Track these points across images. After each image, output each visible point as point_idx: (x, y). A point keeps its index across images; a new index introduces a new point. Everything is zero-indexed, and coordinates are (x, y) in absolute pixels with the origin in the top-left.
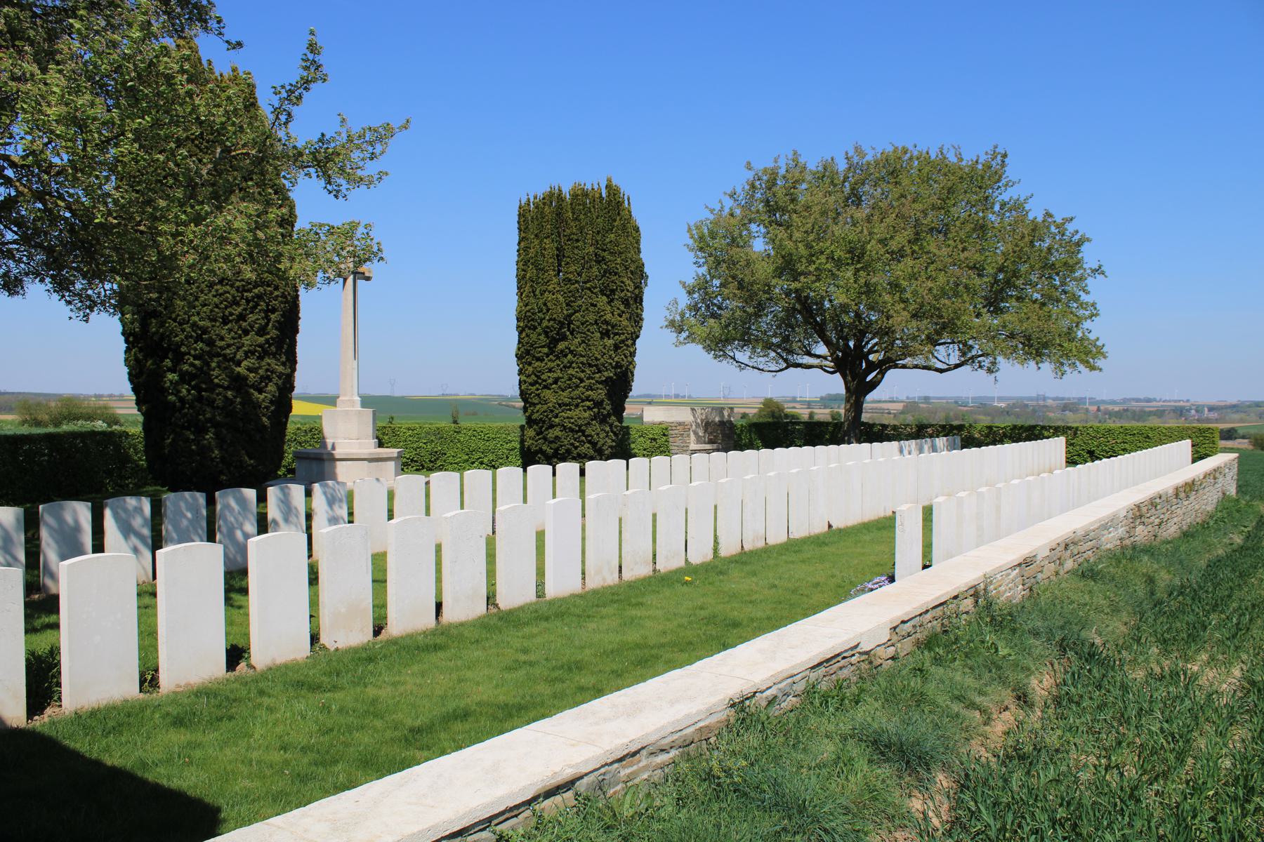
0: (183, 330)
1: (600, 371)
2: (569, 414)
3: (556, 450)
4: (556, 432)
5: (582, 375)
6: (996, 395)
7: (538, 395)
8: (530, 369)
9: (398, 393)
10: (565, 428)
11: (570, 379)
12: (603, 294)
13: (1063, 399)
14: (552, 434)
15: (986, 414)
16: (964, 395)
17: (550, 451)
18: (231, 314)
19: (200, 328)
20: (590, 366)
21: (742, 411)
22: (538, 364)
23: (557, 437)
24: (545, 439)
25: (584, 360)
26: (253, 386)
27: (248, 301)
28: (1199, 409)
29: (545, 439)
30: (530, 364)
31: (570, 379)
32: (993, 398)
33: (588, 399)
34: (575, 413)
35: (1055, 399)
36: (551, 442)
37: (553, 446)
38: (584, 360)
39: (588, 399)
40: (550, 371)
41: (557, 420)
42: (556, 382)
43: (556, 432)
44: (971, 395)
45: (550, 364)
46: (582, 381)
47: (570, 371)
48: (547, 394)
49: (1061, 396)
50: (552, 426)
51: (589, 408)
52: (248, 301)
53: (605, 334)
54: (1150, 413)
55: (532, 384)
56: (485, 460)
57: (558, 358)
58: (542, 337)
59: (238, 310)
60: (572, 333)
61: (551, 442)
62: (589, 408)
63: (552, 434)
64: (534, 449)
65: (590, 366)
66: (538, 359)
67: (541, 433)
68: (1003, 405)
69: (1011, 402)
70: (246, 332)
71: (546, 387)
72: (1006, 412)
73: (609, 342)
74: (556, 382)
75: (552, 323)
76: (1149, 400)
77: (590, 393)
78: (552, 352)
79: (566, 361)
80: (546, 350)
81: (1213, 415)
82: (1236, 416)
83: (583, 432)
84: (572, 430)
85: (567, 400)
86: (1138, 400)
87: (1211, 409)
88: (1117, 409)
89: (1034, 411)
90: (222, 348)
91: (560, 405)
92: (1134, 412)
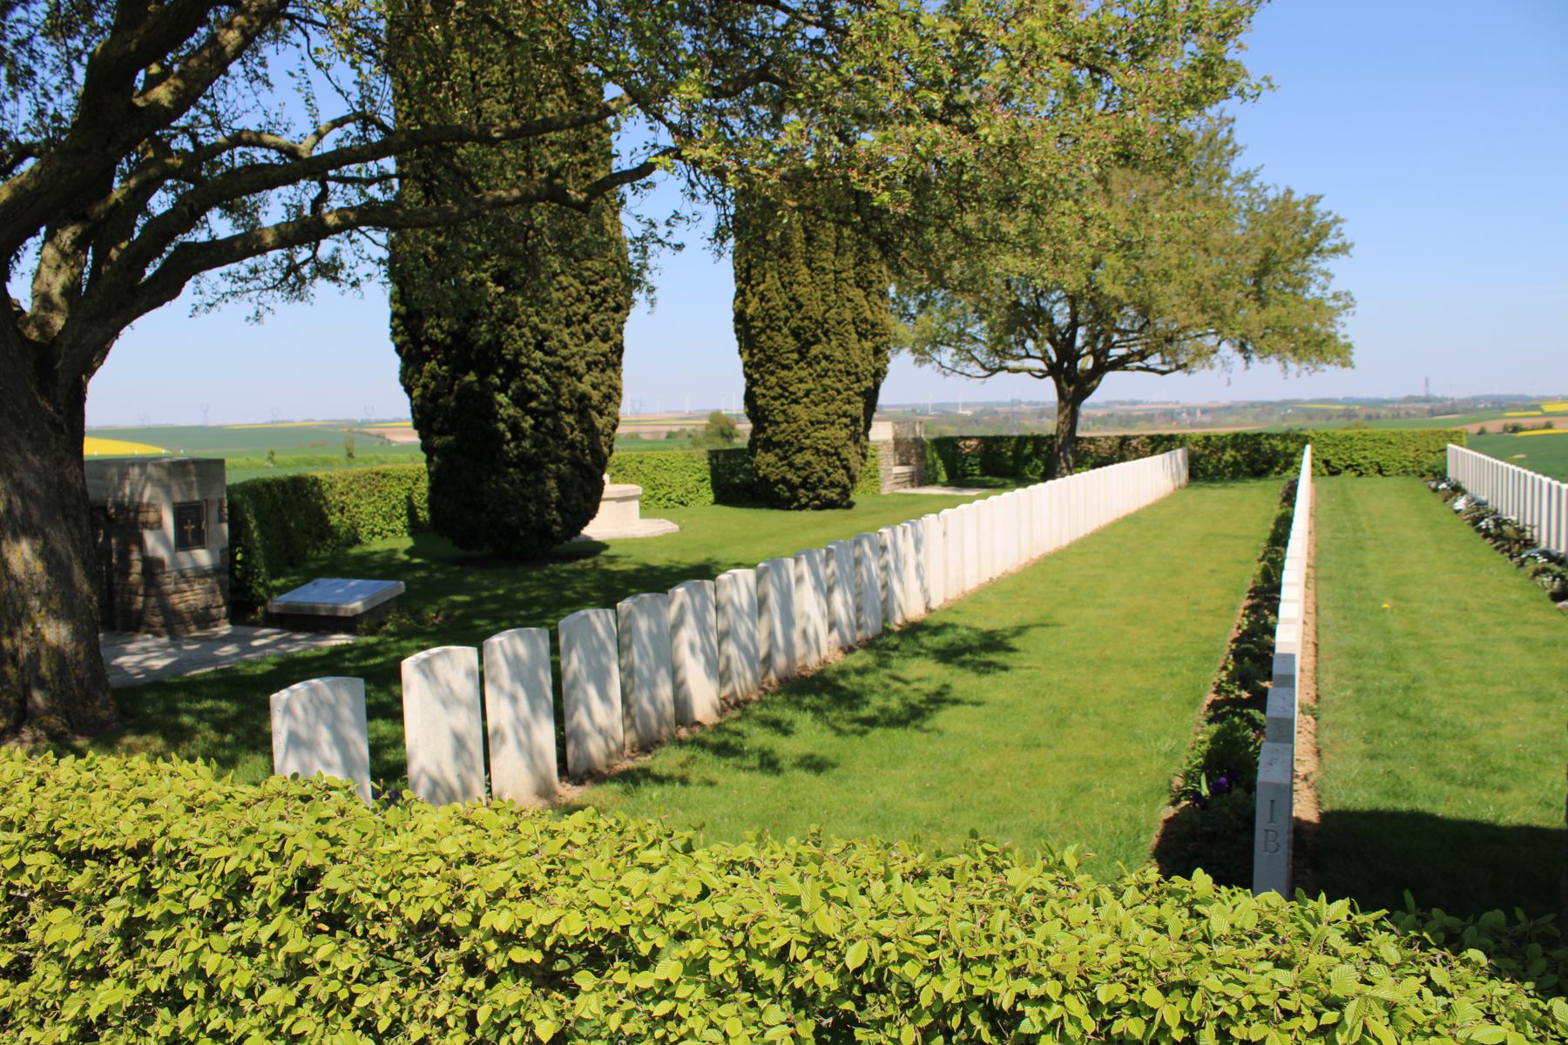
0: (522, 335)
1: (858, 381)
2: (823, 433)
3: (805, 479)
4: (808, 456)
5: (839, 386)
6: (960, 401)
7: (784, 412)
8: (773, 380)
9: (214, 420)
10: (818, 450)
11: (825, 391)
12: (858, 286)
13: (1037, 404)
14: (799, 459)
15: (952, 424)
16: (922, 402)
17: (796, 480)
18: (576, 314)
19: (541, 332)
20: (849, 374)
21: (667, 429)
22: (784, 373)
23: (809, 463)
24: (791, 465)
25: (842, 367)
26: (594, 408)
27: (593, 296)
28: (1191, 412)
29: (791, 465)
30: (772, 373)
31: (825, 391)
32: (956, 405)
33: (845, 415)
34: (831, 432)
35: (1029, 404)
36: (799, 469)
37: (801, 473)
38: (842, 367)
39: (845, 415)
40: (801, 381)
41: (808, 442)
42: (807, 395)
43: (808, 456)
44: (930, 402)
45: (803, 374)
46: (839, 392)
47: (827, 381)
48: (797, 410)
49: (1035, 399)
50: (801, 450)
51: (846, 426)
52: (593, 296)
53: (862, 336)
54: (1138, 418)
55: (774, 399)
56: (673, 496)
57: (810, 365)
58: (790, 340)
59: (582, 309)
60: (826, 333)
61: (799, 469)
62: (846, 426)
63: (799, 459)
64: (773, 478)
65: (849, 374)
66: (785, 367)
67: (786, 458)
68: (969, 412)
69: (978, 409)
70: (588, 337)
71: (796, 402)
72: (974, 420)
73: (868, 345)
74: (807, 395)
75: (806, 322)
76: (1134, 403)
77: (847, 407)
78: (803, 356)
79: (818, 369)
80: (795, 356)
81: (1207, 418)
82: (1231, 419)
83: (838, 454)
84: (827, 453)
85: (822, 417)
86: (1122, 403)
87: (1204, 411)
88: (1099, 413)
89: (1006, 419)
90: (565, 359)
91: (812, 423)
92: (1120, 417)
